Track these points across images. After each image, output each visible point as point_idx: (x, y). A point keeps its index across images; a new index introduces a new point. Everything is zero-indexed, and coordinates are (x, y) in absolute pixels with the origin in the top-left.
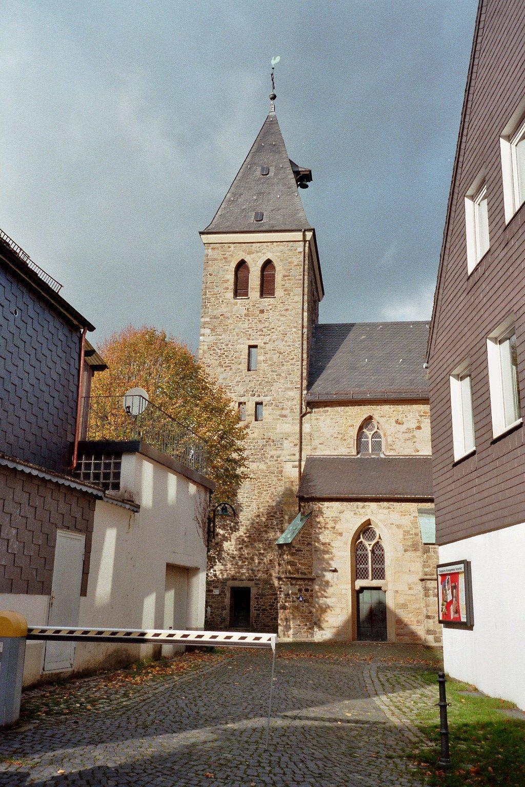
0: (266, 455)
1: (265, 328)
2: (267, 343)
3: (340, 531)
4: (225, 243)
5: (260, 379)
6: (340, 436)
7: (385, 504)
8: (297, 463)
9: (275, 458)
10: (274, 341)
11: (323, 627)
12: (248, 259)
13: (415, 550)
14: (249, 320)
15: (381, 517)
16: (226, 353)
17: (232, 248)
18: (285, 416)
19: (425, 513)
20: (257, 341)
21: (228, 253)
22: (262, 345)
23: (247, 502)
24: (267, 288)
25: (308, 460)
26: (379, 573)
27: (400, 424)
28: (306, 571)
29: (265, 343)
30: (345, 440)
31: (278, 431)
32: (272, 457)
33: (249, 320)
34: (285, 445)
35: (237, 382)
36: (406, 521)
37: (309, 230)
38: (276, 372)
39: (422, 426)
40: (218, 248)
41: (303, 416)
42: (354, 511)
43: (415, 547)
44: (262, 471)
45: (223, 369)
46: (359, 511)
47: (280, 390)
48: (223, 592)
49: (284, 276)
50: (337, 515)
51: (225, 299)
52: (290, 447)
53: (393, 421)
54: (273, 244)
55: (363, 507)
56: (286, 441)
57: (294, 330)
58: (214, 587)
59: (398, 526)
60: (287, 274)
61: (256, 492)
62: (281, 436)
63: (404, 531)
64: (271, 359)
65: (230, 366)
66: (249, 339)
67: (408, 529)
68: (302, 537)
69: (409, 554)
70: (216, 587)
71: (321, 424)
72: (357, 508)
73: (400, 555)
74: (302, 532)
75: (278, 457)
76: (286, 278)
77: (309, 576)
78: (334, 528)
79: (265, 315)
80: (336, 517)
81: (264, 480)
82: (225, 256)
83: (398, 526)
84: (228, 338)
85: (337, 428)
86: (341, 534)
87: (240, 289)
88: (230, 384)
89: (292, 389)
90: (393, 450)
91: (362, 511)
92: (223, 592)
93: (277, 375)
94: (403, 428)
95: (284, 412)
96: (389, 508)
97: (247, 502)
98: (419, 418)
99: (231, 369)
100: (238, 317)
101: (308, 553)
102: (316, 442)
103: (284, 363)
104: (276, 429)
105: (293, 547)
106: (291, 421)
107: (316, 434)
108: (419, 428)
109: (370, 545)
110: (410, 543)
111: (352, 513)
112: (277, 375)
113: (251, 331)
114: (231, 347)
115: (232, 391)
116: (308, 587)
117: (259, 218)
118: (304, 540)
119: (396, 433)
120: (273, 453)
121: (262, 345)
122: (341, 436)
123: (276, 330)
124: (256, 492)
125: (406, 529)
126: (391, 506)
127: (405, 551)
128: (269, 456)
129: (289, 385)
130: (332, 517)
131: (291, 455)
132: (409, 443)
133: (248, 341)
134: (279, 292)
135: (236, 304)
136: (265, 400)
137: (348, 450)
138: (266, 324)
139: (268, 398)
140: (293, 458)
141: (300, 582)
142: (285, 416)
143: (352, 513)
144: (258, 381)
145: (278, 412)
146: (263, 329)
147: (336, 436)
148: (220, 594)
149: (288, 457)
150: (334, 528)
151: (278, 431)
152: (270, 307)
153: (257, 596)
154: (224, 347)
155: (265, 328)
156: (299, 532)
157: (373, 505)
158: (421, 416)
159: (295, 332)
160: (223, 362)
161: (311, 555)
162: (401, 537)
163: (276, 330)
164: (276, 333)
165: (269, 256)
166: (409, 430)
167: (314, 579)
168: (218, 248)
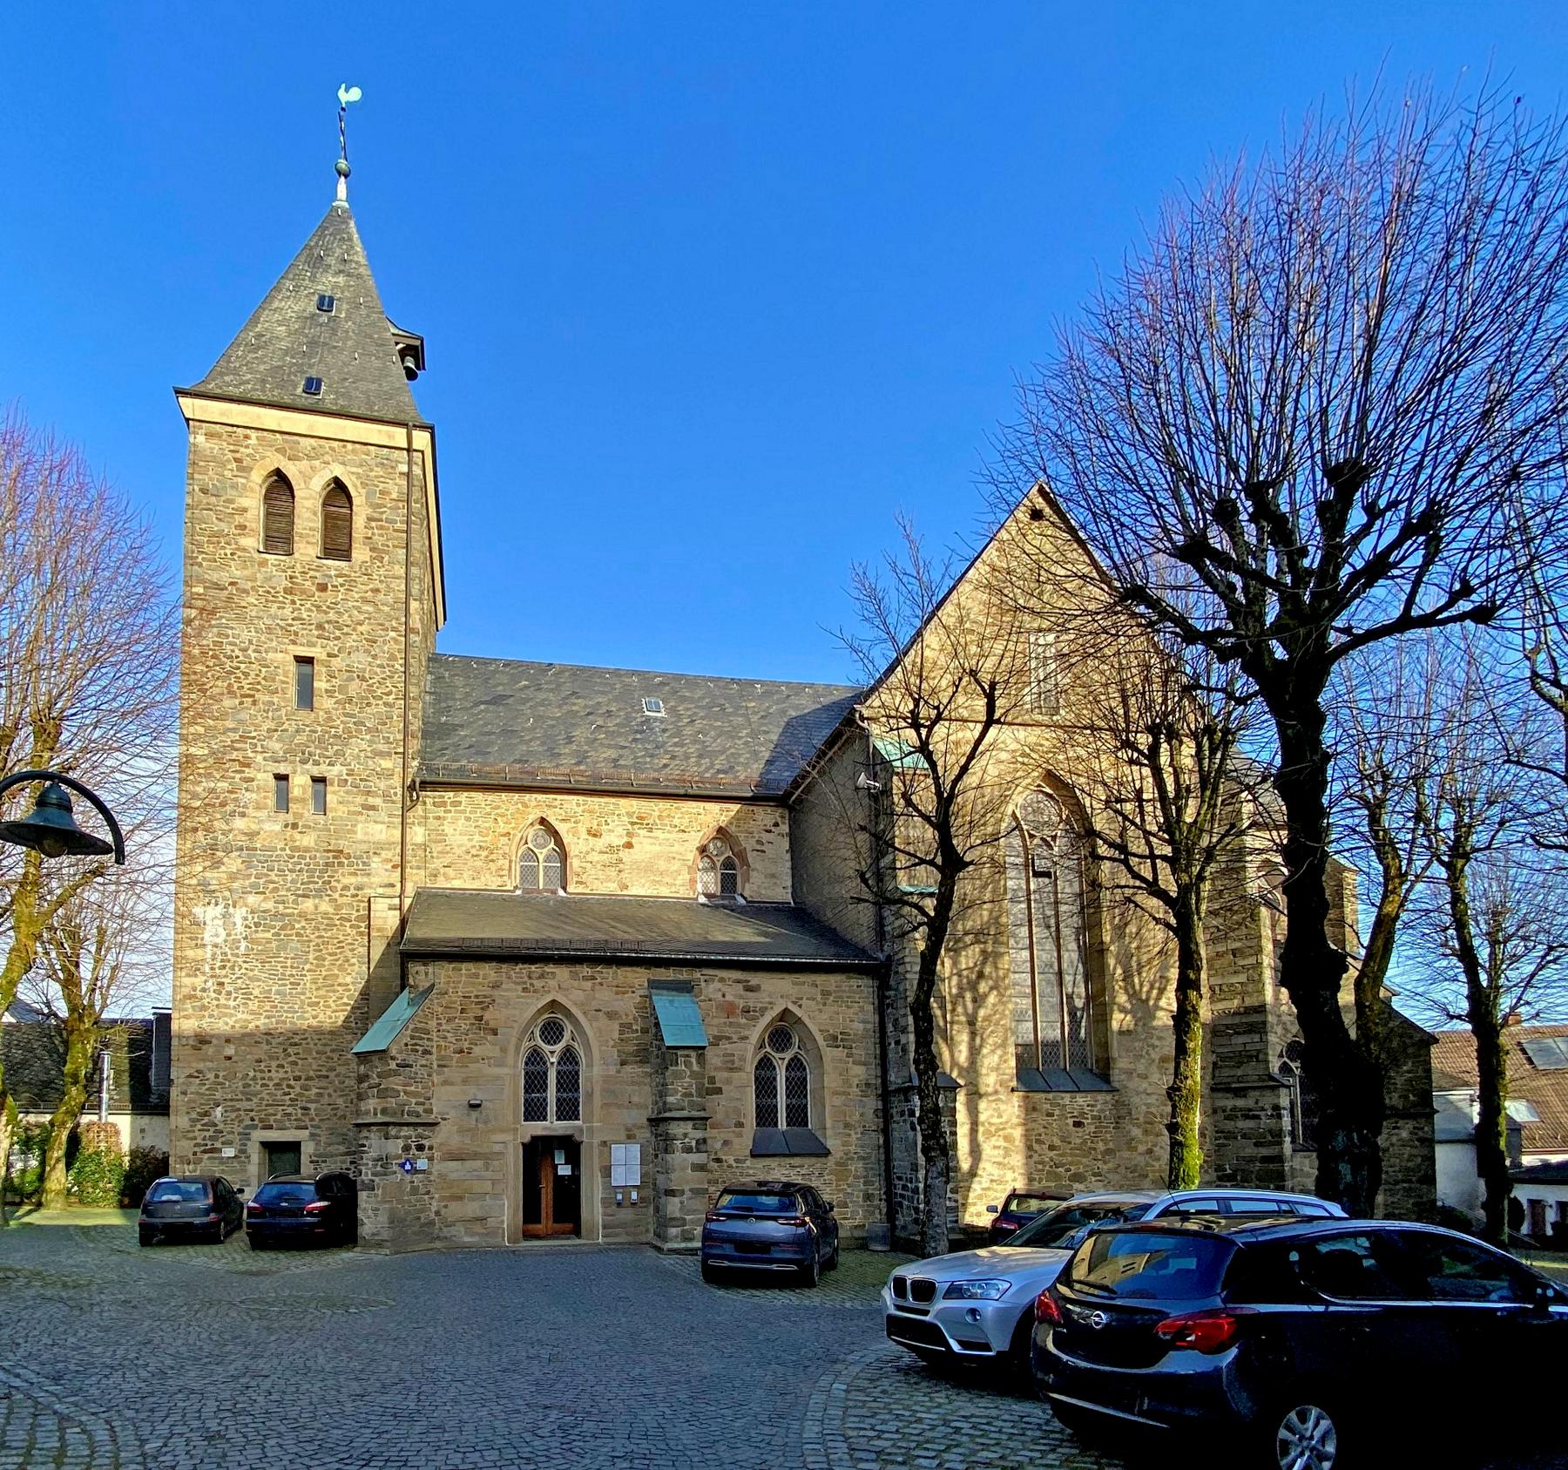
0: (333, 884)
1: (328, 622)
2: (336, 656)
3: (492, 1024)
4: (238, 426)
5: (319, 729)
6: (485, 853)
7: (585, 970)
8: (397, 901)
9: (353, 891)
10: (349, 653)
11: (316, 705)
12: (290, 470)
13: (641, 1061)
14: (293, 602)
15: (578, 995)
16: (243, 666)
17: (253, 441)
18: (373, 808)
19: (663, 988)
20: (313, 649)
21: (242, 450)
22: (324, 657)
23: (292, 975)
24: (337, 544)
25: (418, 895)
26: (568, 1110)
27: (595, 835)
28: (420, 1109)
29: (329, 655)
30: (492, 861)
31: (360, 836)
32: (346, 888)
33: (293, 602)
34: (373, 865)
35: (269, 731)
36: (628, 1005)
37: (423, 427)
38: (353, 716)
39: (634, 841)
40: (219, 436)
41: (405, 810)
42: (525, 983)
43: (642, 1056)
44: (325, 915)
45: (237, 702)
46: (532, 984)
47: (362, 754)
48: (243, 1151)
49: (370, 519)
50: (489, 992)
51: (238, 549)
52: (381, 872)
53: (582, 829)
54: (344, 447)
55: (542, 976)
56: (376, 859)
57: (393, 634)
58: (223, 1143)
59: (611, 1015)
60: (376, 515)
61: (311, 957)
62: (365, 847)
63: (621, 1025)
64: (342, 689)
65: (253, 696)
66: (294, 643)
67: (630, 1019)
68: (412, 1038)
69: (628, 1068)
70: (229, 1143)
71: (448, 829)
72: (530, 978)
73: (612, 1070)
74: (411, 1026)
75: (358, 888)
76: (373, 524)
77: (425, 1119)
78: (480, 1019)
79: (329, 596)
80: (485, 997)
81: (329, 934)
82: (238, 455)
83: (611, 1015)
84: (245, 635)
85: (477, 837)
86: (495, 1032)
87: (279, 538)
88: (254, 734)
89: (389, 754)
90: (581, 883)
91: (538, 984)
92: (243, 1151)
93: (355, 723)
94: (600, 843)
95: (371, 801)
96: (594, 978)
97: (292, 975)
98: (629, 827)
99: (254, 703)
100: (268, 592)
101: (424, 1071)
102: (437, 864)
103: (372, 700)
104: (356, 833)
105: (393, 1058)
106: (387, 819)
107: (436, 848)
108: (629, 845)
109: (552, 1053)
110: (632, 1049)
111: (520, 988)
112: (355, 723)
113: (297, 626)
114: (253, 655)
115: (259, 749)
116: (424, 1142)
117: (313, 386)
118: (416, 1044)
119: (588, 853)
120: (346, 881)
121: (324, 657)
122: (486, 853)
123: (354, 630)
124: (311, 957)
125: (624, 1020)
126: (596, 975)
127: (623, 1063)
128: (339, 886)
129: (382, 747)
130: (477, 997)
131: (386, 886)
132: (613, 872)
133: (291, 647)
134: (360, 553)
135: (263, 563)
136: (332, 772)
137: (499, 881)
138: (332, 616)
139: (337, 769)
140: (389, 891)
141: (405, 1131)
142: (373, 808)
143: (520, 988)
144: (315, 732)
145: (360, 800)
146: (326, 626)
147: (474, 852)
148: (236, 1157)
149: (381, 891)
150: (480, 1019)
151: (360, 836)
152: (341, 580)
153: (314, 1158)
154: (237, 652)
155: (328, 622)
156: (406, 1027)
157: (562, 973)
158: (633, 824)
159: (393, 638)
160: (236, 686)
161: (430, 1075)
162: (616, 1035)
163: (354, 630)
164: (354, 637)
165: (338, 471)
166: (611, 849)
167: (437, 1124)
168: (219, 436)
